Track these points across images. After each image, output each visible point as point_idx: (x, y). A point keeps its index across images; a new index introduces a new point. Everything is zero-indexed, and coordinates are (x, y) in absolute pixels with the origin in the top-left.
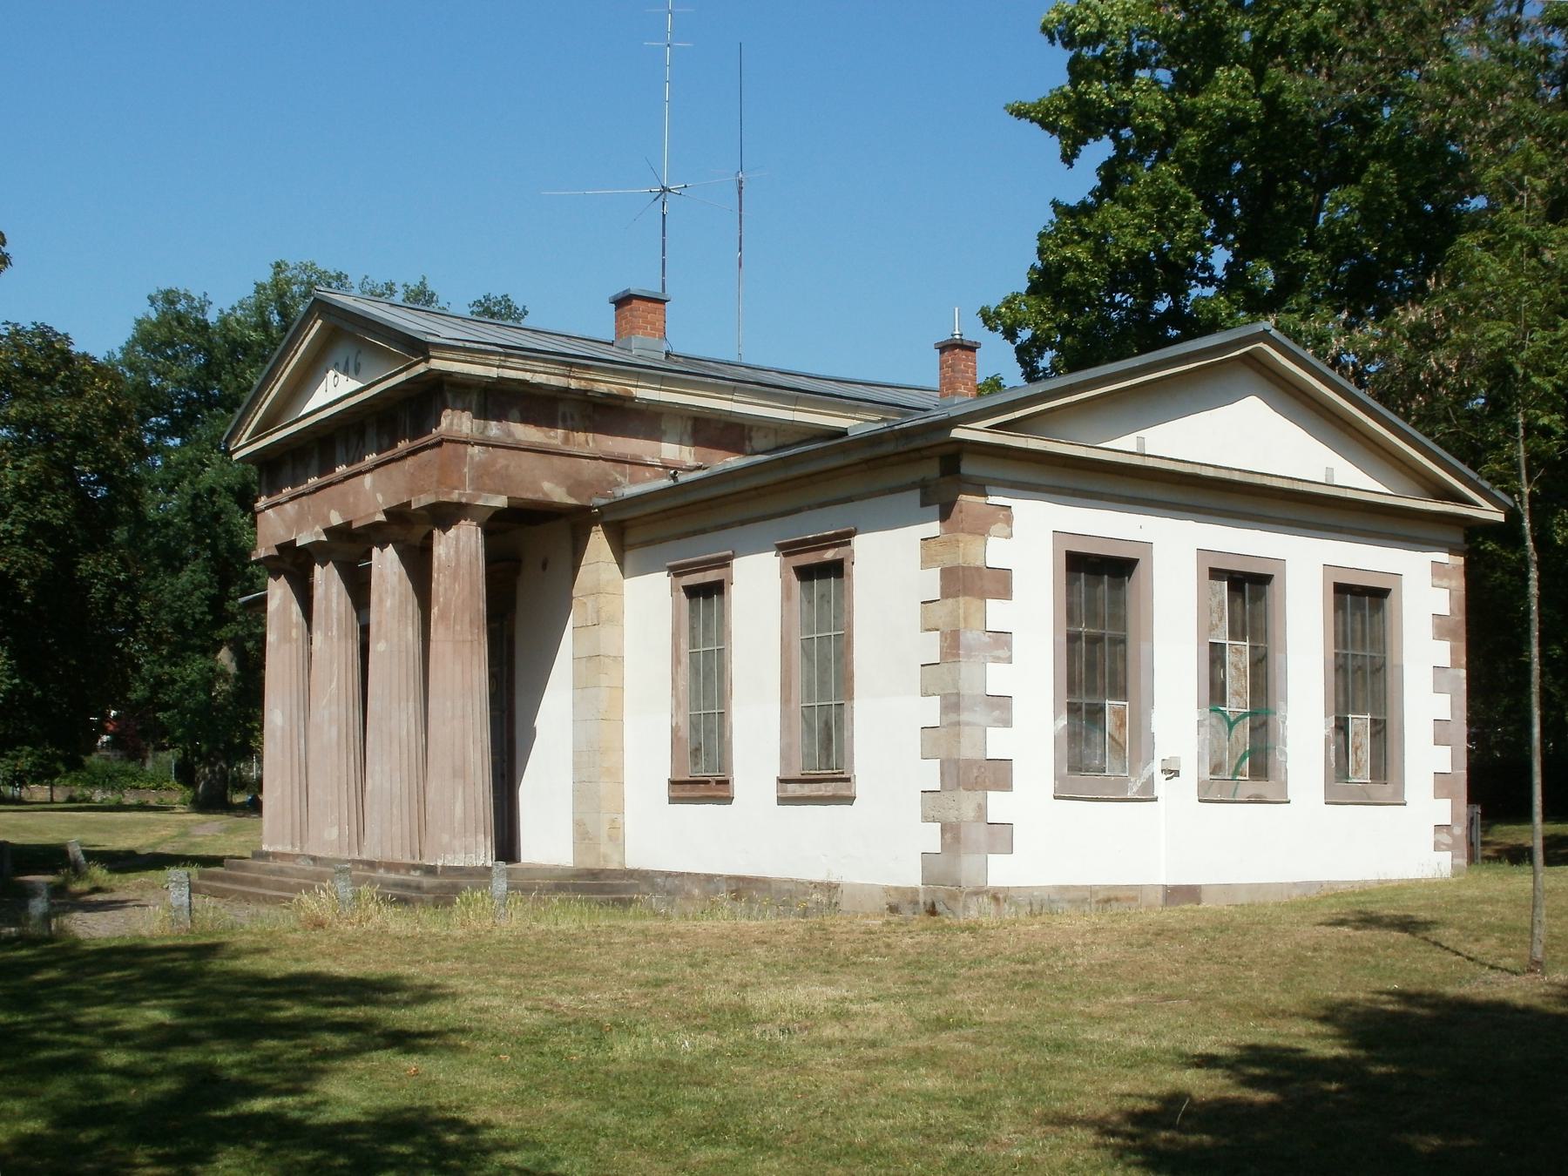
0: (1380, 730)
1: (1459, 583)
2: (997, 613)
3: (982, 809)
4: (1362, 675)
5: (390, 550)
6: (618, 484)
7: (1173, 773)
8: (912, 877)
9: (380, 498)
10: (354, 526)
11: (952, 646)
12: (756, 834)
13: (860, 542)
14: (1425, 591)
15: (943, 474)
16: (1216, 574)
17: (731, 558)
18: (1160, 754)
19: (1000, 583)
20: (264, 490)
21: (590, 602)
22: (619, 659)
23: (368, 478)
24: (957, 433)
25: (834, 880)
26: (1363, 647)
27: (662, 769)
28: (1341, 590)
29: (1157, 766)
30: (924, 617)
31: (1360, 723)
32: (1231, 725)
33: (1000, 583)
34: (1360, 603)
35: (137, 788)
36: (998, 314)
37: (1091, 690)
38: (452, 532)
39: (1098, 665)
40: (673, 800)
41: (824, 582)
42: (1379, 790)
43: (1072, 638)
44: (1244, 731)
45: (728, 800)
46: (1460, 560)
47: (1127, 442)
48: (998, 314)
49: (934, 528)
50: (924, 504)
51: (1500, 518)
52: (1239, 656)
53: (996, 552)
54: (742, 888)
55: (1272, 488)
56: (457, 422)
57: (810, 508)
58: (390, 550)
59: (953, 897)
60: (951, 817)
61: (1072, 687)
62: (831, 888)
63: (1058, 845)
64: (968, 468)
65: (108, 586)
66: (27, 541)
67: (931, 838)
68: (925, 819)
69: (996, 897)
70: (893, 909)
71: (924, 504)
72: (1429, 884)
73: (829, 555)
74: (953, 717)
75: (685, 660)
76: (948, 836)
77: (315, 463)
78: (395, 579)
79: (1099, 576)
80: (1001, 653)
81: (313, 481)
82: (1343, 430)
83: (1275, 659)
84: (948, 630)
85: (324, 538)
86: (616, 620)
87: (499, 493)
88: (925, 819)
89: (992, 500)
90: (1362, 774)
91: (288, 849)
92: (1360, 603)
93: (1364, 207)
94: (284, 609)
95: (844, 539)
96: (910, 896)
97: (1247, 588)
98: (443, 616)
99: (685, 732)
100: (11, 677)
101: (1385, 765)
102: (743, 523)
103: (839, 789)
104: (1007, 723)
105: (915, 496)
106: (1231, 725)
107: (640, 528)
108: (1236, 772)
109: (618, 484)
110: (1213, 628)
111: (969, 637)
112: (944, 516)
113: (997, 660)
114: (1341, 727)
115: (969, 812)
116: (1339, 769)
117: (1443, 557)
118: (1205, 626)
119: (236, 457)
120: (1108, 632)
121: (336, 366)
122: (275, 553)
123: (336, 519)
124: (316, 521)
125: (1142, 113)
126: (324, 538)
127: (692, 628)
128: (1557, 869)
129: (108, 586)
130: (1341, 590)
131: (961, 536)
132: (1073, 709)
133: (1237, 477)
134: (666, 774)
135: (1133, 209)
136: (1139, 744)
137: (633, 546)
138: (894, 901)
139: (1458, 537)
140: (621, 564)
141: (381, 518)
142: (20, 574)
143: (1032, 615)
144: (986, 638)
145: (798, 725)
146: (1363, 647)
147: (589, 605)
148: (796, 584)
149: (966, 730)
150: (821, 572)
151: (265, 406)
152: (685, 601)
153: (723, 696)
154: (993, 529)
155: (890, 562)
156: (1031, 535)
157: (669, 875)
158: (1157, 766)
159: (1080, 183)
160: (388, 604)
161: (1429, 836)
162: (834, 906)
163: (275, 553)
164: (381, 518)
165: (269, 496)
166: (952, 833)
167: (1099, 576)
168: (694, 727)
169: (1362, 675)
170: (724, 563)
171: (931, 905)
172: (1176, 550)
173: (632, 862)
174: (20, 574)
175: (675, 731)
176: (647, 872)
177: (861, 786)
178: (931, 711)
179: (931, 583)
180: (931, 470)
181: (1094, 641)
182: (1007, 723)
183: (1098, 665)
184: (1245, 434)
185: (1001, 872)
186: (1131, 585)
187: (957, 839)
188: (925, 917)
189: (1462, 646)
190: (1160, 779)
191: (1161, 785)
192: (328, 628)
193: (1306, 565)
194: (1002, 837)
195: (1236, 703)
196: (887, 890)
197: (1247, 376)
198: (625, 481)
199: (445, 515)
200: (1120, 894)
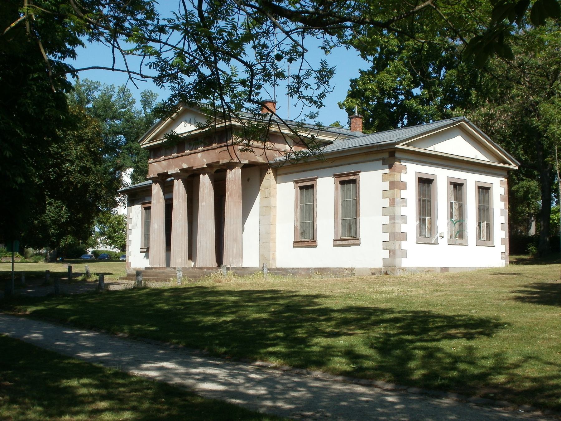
0: (488, 226)
1: (506, 186)
2: (404, 194)
3: (400, 246)
4: (484, 211)
5: (207, 175)
6: (275, 157)
7: (442, 237)
8: (379, 264)
9: (205, 160)
10: (194, 168)
11: (393, 202)
12: (326, 254)
13: (361, 174)
14: (498, 187)
15: (390, 157)
16: (451, 183)
17: (317, 178)
18: (439, 232)
19: (404, 185)
20: (152, 156)
21: (267, 191)
22: (275, 207)
23: (199, 155)
24: (397, 146)
25: (353, 267)
26: (484, 203)
27: (291, 238)
28: (479, 187)
29: (438, 235)
30: (383, 195)
31: (483, 224)
32: (454, 224)
33: (404, 185)
34: (483, 190)
35: (6, 257)
36: (344, 104)
37: (423, 215)
38: (233, 171)
39: (425, 207)
40: (294, 247)
41: (349, 185)
42: (489, 243)
43: (420, 200)
44: (457, 225)
45: (316, 246)
46: (506, 180)
47: (431, 148)
48: (344, 104)
49: (387, 171)
50: (383, 164)
51: (517, 168)
52: (456, 206)
53: (404, 177)
54: (321, 271)
55: (463, 160)
56: (235, 139)
57: (345, 165)
58: (207, 175)
59: (393, 269)
60: (393, 248)
61: (420, 214)
62: (352, 269)
63: (420, 257)
64: (397, 155)
65: (95, 185)
66: (79, 172)
67: (386, 254)
68: (384, 249)
69: (404, 269)
70: (373, 274)
71: (383, 164)
72: (502, 268)
73: (351, 178)
74: (393, 221)
75: (299, 207)
76: (391, 253)
77: (176, 149)
78: (208, 184)
79: (425, 183)
80: (405, 204)
81: (175, 155)
82: (480, 145)
83: (464, 207)
84: (391, 198)
85: (179, 172)
86: (275, 196)
87: (246, 159)
88: (384, 249)
89: (402, 163)
90: (484, 238)
91: (158, 266)
92: (483, 190)
93: (458, 76)
94: (158, 193)
95: (357, 173)
96: (380, 271)
97: (457, 186)
98: (230, 194)
99: (299, 228)
100: (67, 213)
101: (489, 236)
102: (321, 168)
103: (356, 242)
104: (406, 223)
105: (381, 162)
106: (454, 224)
107: (281, 170)
108: (456, 237)
109: (275, 157)
110: (450, 198)
111: (397, 200)
112: (390, 167)
113: (403, 206)
114: (479, 225)
115: (397, 247)
116: (479, 237)
117: (502, 179)
118: (449, 198)
119: (142, 147)
120: (427, 199)
121: (186, 121)
122: (157, 176)
123: (185, 166)
124: (176, 166)
125: (391, 46)
126: (179, 172)
127: (301, 198)
128: (512, 265)
129: (95, 185)
130: (479, 187)
131: (396, 173)
132: (420, 219)
133: (458, 157)
134: (293, 240)
135: (390, 74)
136: (433, 229)
137: (280, 175)
138: (373, 272)
139: (506, 173)
140: (276, 180)
141: (205, 166)
142: (78, 182)
143: (411, 194)
144: (401, 200)
145: (340, 225)
146: (484, 203)
147: (266, 192)
148: (339, 186)
149: (396, 225)
150: (349, 182)
151: (156, 132)
152: (299, 190)
153: (314, 217)
154: (403, 171)
155: (372, 181)
156: (411, 172)
157: (293, 269)
158: (438, 235)
159: (367, 65)
160: (206, 191)
161: (500, 256)
162: (352, 274)
163: (157, 176)
164: (205, 166)
165: (154, 159)
166: (392, 253)
167: (425, 183)
168: (302, 226)
169: (484, 211)
170: (315, 179)
171: (387, 272)
172: (443, 176)
173: (278, 266)
174: (78, 182)
175: (296, 227)
176: (285, 268)
177: (362, 241)
178: (386, 220)
179: (386, 185)
180: (386, 155)
181: (424, 201)
182: (406, 223)
183: (425, 207)
184: (457, 146)
185: (405, 263)
186: (432, 186)
187: (394, 254)
188: (385, 276)
189: (507, 203)
190: (439, 238)
191: (440, 240)
192: (179, 199)
193: (472, 180)
194: (404, 253)
195: (456, 218)
196: (371, 269)
197: (458, 131)
198: (277, 156)
199: (231, 166)
200: (431, 269)
